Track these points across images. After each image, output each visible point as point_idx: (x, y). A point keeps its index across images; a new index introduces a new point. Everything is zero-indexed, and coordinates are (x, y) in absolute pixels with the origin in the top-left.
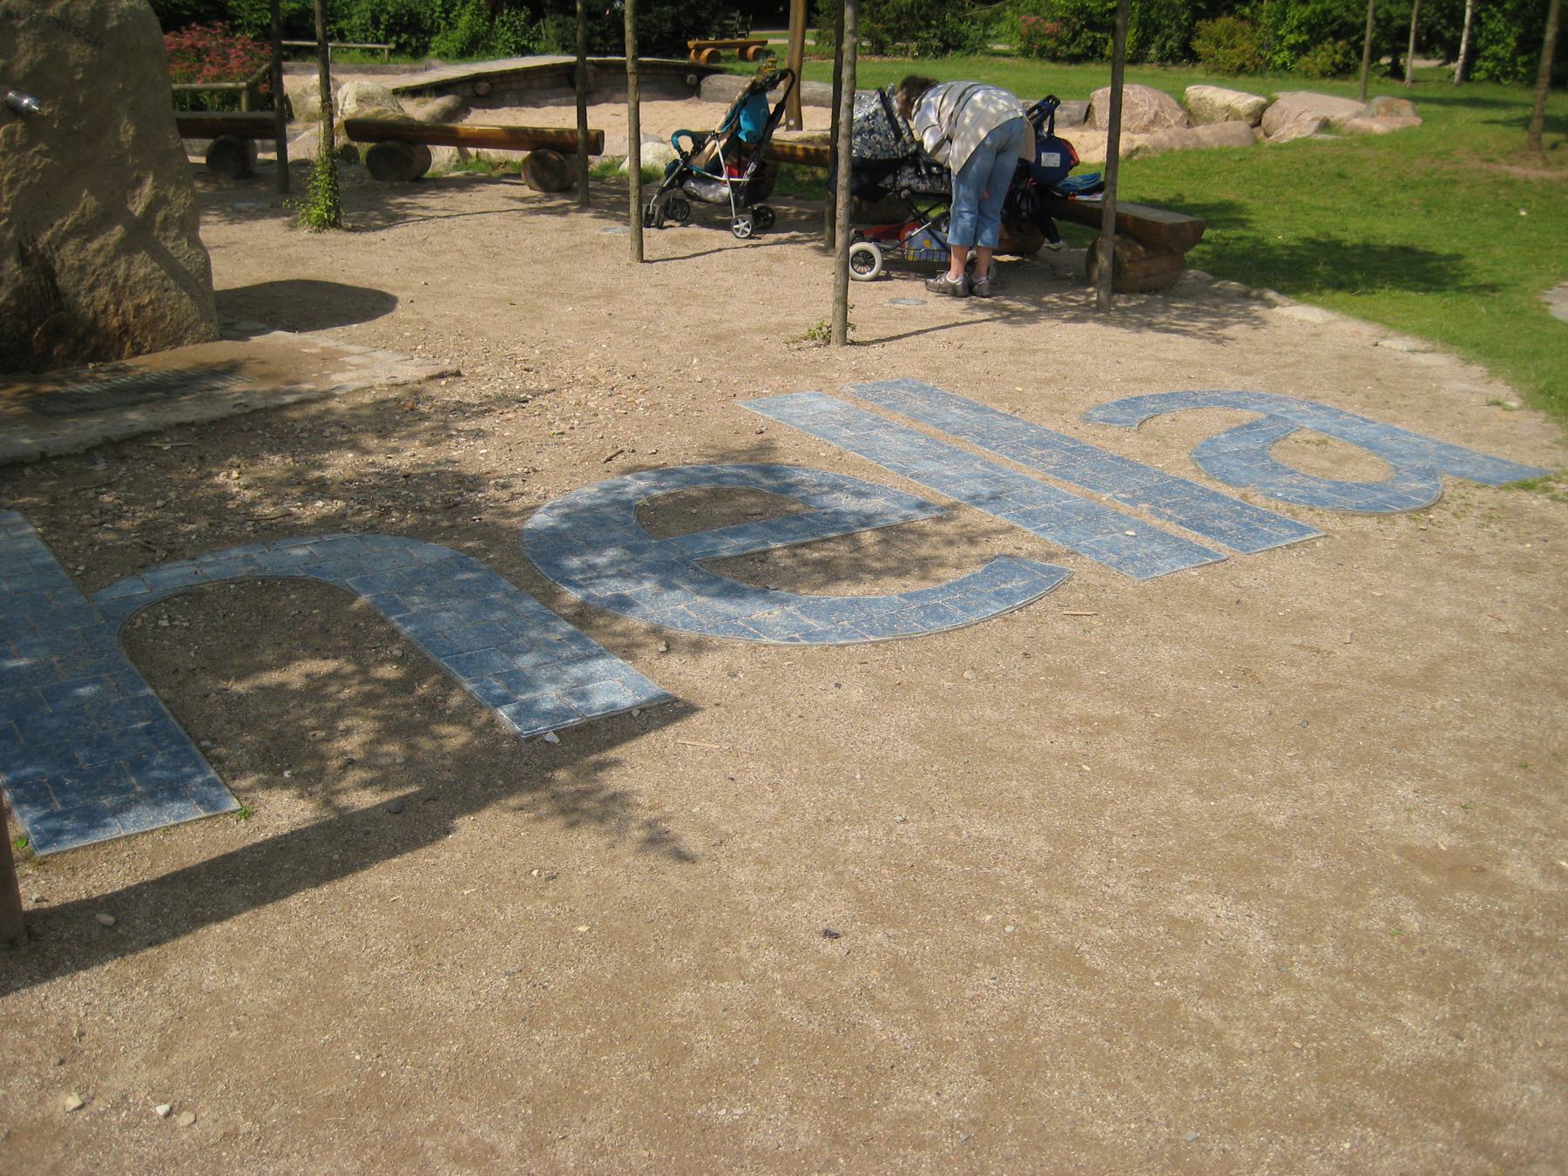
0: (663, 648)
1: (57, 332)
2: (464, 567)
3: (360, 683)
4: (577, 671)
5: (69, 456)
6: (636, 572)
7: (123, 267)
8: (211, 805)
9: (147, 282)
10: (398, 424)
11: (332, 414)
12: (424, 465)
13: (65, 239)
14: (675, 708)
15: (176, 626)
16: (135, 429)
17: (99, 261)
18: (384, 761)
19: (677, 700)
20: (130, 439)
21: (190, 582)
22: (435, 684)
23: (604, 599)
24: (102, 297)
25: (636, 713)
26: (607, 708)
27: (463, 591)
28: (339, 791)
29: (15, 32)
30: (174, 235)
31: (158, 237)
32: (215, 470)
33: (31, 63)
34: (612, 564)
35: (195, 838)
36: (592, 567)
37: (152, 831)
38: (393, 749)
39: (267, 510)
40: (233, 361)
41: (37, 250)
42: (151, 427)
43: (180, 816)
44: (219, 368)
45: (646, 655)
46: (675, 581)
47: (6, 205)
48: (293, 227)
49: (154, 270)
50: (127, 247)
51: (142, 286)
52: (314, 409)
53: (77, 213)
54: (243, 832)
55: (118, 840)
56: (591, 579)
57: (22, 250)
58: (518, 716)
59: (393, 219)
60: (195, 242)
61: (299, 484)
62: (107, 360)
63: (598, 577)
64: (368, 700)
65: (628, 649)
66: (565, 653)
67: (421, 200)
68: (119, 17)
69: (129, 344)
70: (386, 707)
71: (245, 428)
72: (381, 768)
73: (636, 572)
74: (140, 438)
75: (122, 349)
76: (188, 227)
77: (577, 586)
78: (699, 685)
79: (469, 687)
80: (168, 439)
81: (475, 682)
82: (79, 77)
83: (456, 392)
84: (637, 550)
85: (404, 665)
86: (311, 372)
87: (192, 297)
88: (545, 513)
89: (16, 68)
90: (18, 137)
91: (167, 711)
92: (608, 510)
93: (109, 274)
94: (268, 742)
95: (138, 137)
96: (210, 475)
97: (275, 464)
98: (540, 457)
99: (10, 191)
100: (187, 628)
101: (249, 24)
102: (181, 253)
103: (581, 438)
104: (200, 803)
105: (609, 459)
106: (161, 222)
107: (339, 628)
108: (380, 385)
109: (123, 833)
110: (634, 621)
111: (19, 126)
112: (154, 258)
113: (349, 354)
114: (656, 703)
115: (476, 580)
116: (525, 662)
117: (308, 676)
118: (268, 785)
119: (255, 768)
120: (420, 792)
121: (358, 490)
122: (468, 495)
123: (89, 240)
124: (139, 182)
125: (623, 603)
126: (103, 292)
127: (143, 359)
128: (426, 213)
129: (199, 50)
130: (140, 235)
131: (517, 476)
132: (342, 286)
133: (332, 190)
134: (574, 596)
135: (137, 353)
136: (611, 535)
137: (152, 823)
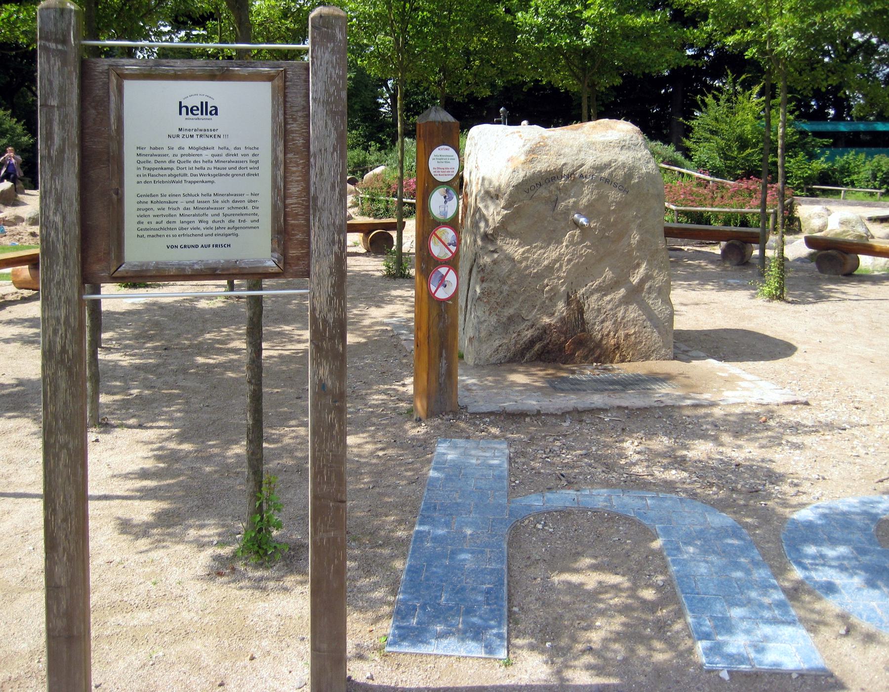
0: (843, 631)
1: (580, 343)
2: (735, 534)
3: (627, 597)
4: (767, 630)
5: (552, 415)
6: (854, 568)
7: (622, 311)
8: (490, 649)
9: (634, 322)
10: (751, 430)
11: (712, 417)
12: (753, 460)
13: (592, 294)
14: (827, 682)
15: (546, 530)
16: (593, 406)
17: (609, 307)
18: (609, 655)
19: (831, 675)
20: (589, 411)
21: (567, 504)
22: (672, 611)
23: (816, 582)
24: (607, 327)
25: (794, 676)
26: (774, 665)
27: (724, 552)
28: (571, 667)
29: (583, 184)
30: (654, 296)
31: (645, 297)
32: (627, 438)
33: (589, 200)
34: (838, 558)
35: (471, 668)
36: (822, 556)
37: (451, 656)
38: (619, 650)
39: (639, 470)
40: (669, 374)
41: (576, 298)
42: (602, 406)
43: (470, 651)
44: (660, 376)
45: (826, 633)
46: (879, 583)
47: (564, 272)
48: (753, 297)
49: (639, 315)
50: (626, 301)
51: (631, 323)
52: (702, 411)
53: (601, 280)
54: (499, 675)
55: (430, 655)
56: (817, 565)
57: (569, 297)
58: (709, 651)
59: (820, 298)
60: (668, 302)
61: (670, 456)
62: (603, 363)
63: (824, 565)
64: (625, 610)
65: (814, 626)
66: (767, 614)
67: (843, 288)
68: (639, 177)
69: (618, 355)
70: (633, 618)
71: (657, 416)
72: (605, 659)
73: (854, 568)
74: (593, 411)
75: (614, 358)
76: (664, 293)
77: (804, 567)
78: (856, 669)
79: (690, 620)
80: (609, 415)
81: (695, 618)
82: (613, 208)
83: (804, 416)
84: (862, 551)
85: (661, 592)
86: (713, 387)
87: (659, 333)
88: (811, 510)
89: (581, 203)
90: (576, 237)
91: (506, 582)
92: (858, 517)
93: (613, 315)
94: (550, 620)
95: (641, 242)
96: (623, 441)
97: (662, 443)
98: (833, 470)
99: (567, 265)
100: (551, 533)
101: (796, 176)
102: (656, 307)
103: (870, 461)
104: (486, 647)
105: (882, 481)
106: (648, 289)
107: (636, 556)
108: (751, 403)
109: (435, 652)
110: (831, 605)
111: (578, 232)
112: (640, 309)
113: (743, 380)
114: (814, 673)
115: (738, 546)
116: (736, 613)
117: (600, 583)
118: (532, 648)
119: (533, 635)
120: (618, 685)
121: (702, 470)
122: (768, 486)
123: (605, 295)
124: (638, 266)
125: (830, 588)
126: (608, 324)
127: (625, 365)
128: (844, 296)
129: (751, 190)
130: (635, 295)
131: (809, 480)
132: (767, 337)
133: (779, 277)
134: (797, 574)
135: (623, 361)
136: (851, 536)
137: (453, 650)
